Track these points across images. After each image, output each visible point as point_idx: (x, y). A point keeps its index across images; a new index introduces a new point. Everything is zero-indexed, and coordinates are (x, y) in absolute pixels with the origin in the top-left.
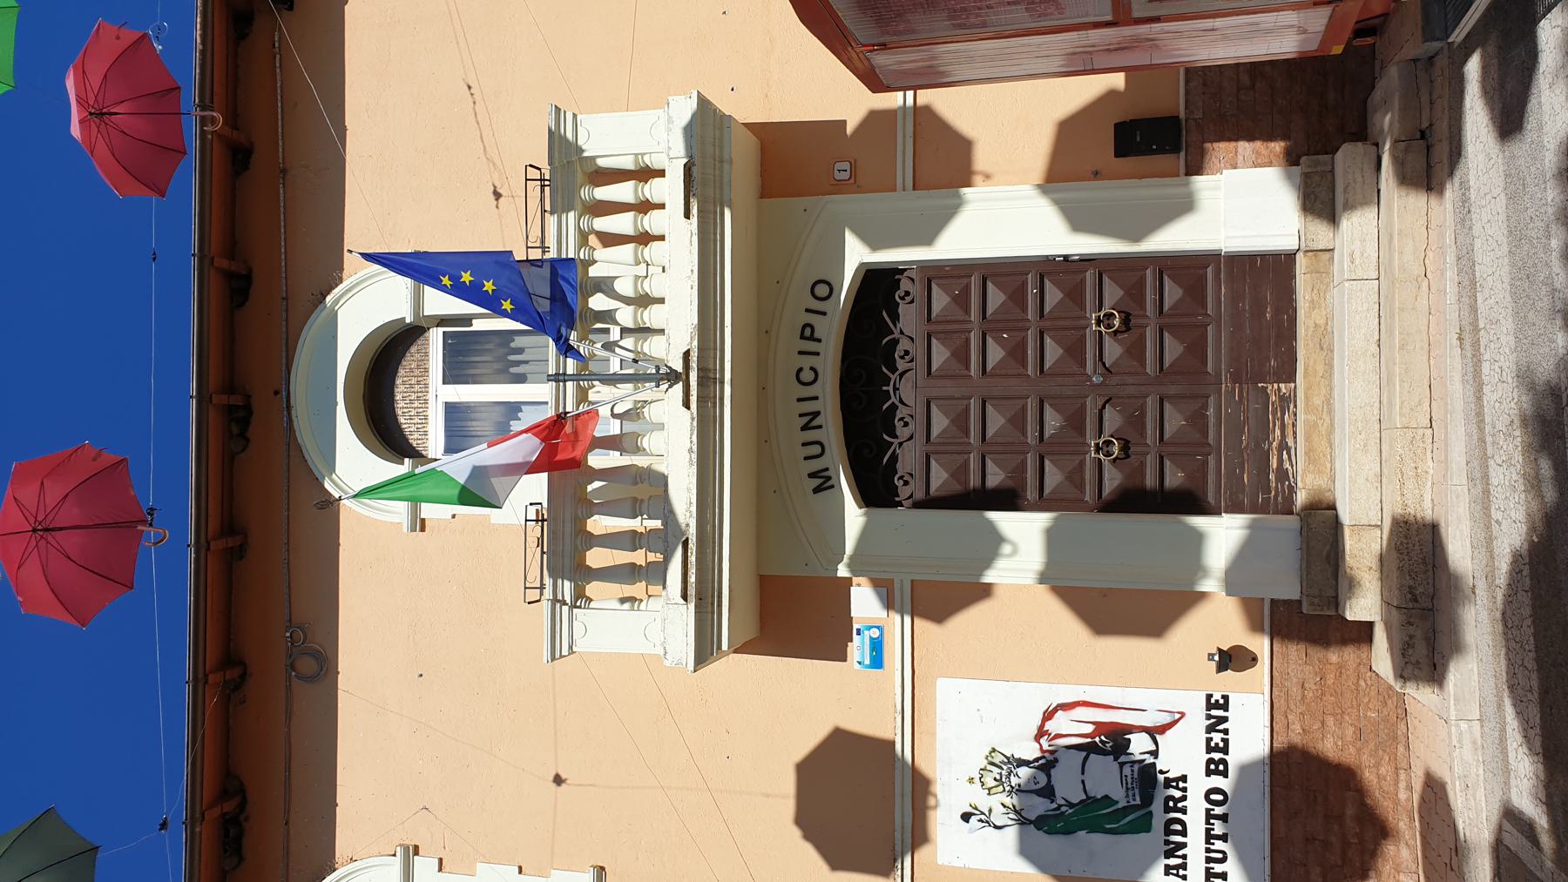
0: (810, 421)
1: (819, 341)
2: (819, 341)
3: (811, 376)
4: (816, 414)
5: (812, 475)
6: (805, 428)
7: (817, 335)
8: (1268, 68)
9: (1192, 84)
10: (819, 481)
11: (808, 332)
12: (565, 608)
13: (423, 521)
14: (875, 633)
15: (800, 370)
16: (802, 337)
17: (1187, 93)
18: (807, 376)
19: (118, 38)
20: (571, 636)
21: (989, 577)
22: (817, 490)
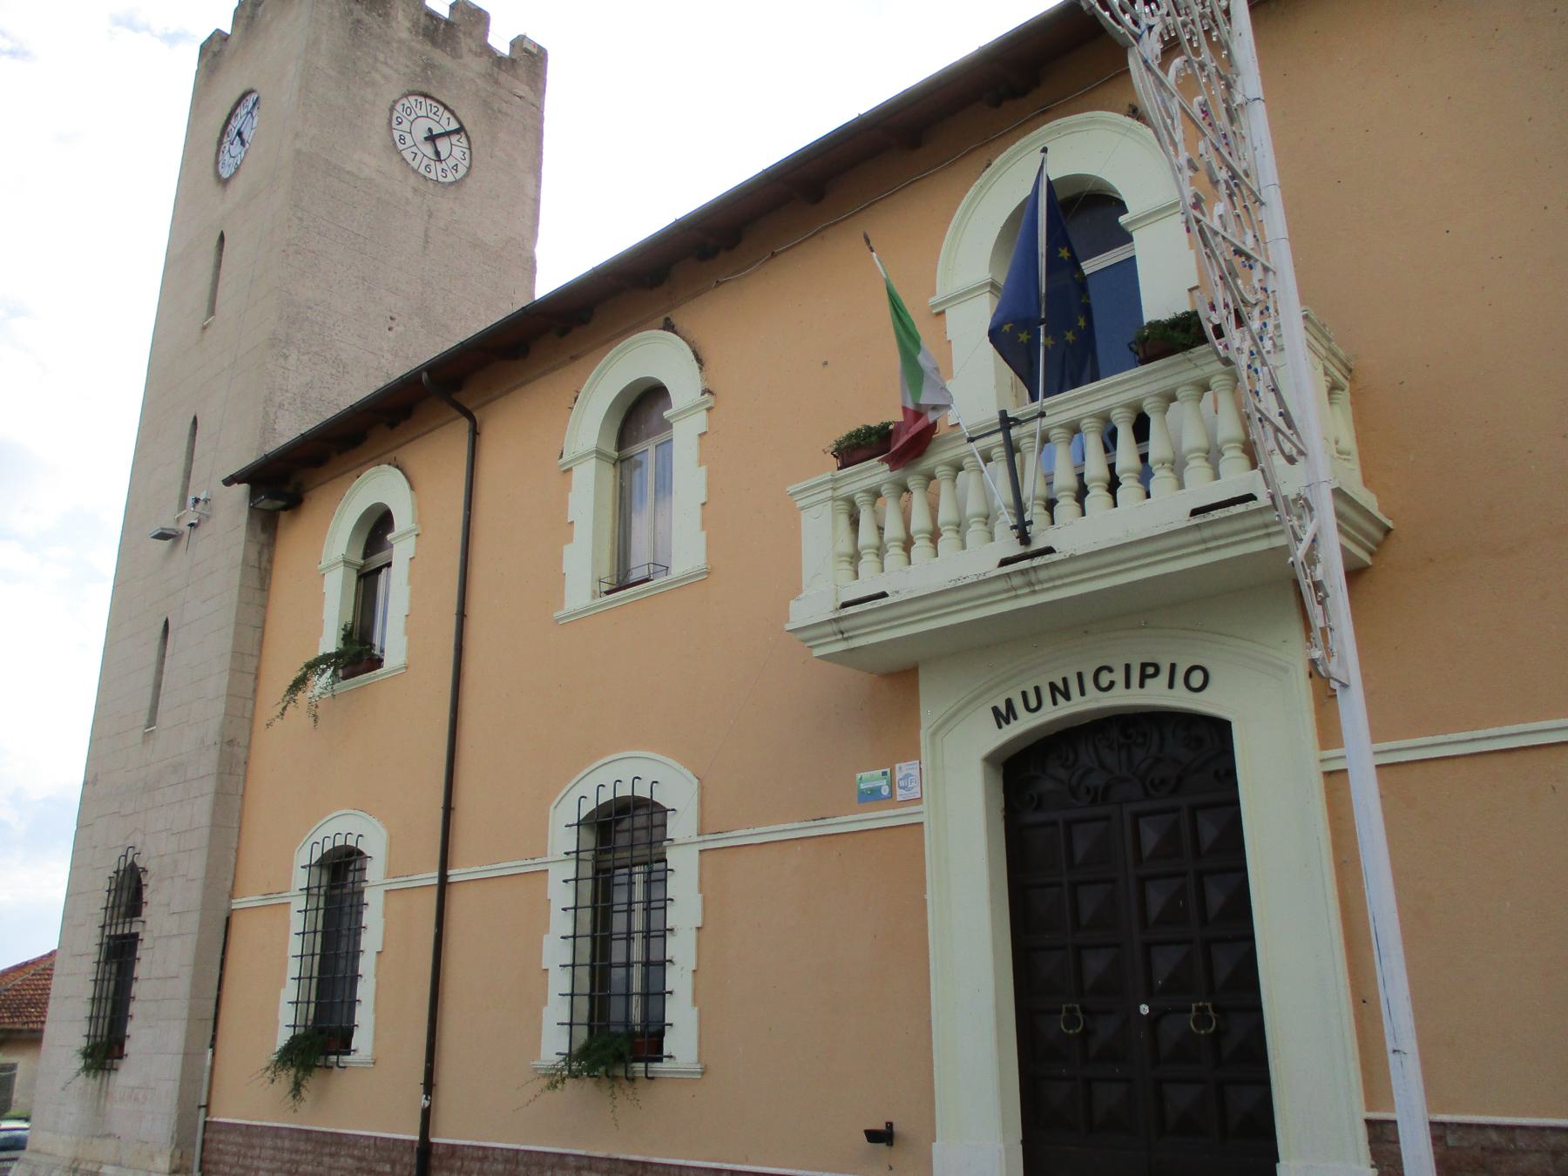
0: (1060, 691)
1: (1142, 685)
2: (1142, 685)
3: (1104, 682)
4: (1067, 697)
5: (1009, 703)
6: (1053, 687)
7: (1148, 682)
8: (1224, 966)
9: (1494, 1136)
10: (1003, 710)
11: (1150, 670)
12: (829, 493)
13: (943, 312)
14: (885, 791)
15: (1110, 670)
16: (1144, 666)
17: (1481, 1127)
18: (1105, 679)
19: (1045, 150)
20: (811, 506)
21: (704, 468)
22: (995, 710)
